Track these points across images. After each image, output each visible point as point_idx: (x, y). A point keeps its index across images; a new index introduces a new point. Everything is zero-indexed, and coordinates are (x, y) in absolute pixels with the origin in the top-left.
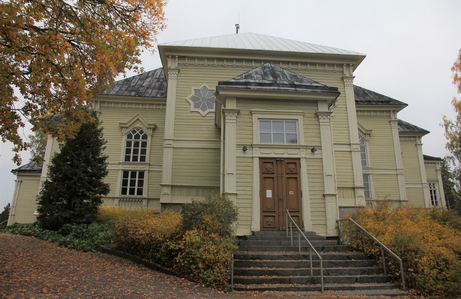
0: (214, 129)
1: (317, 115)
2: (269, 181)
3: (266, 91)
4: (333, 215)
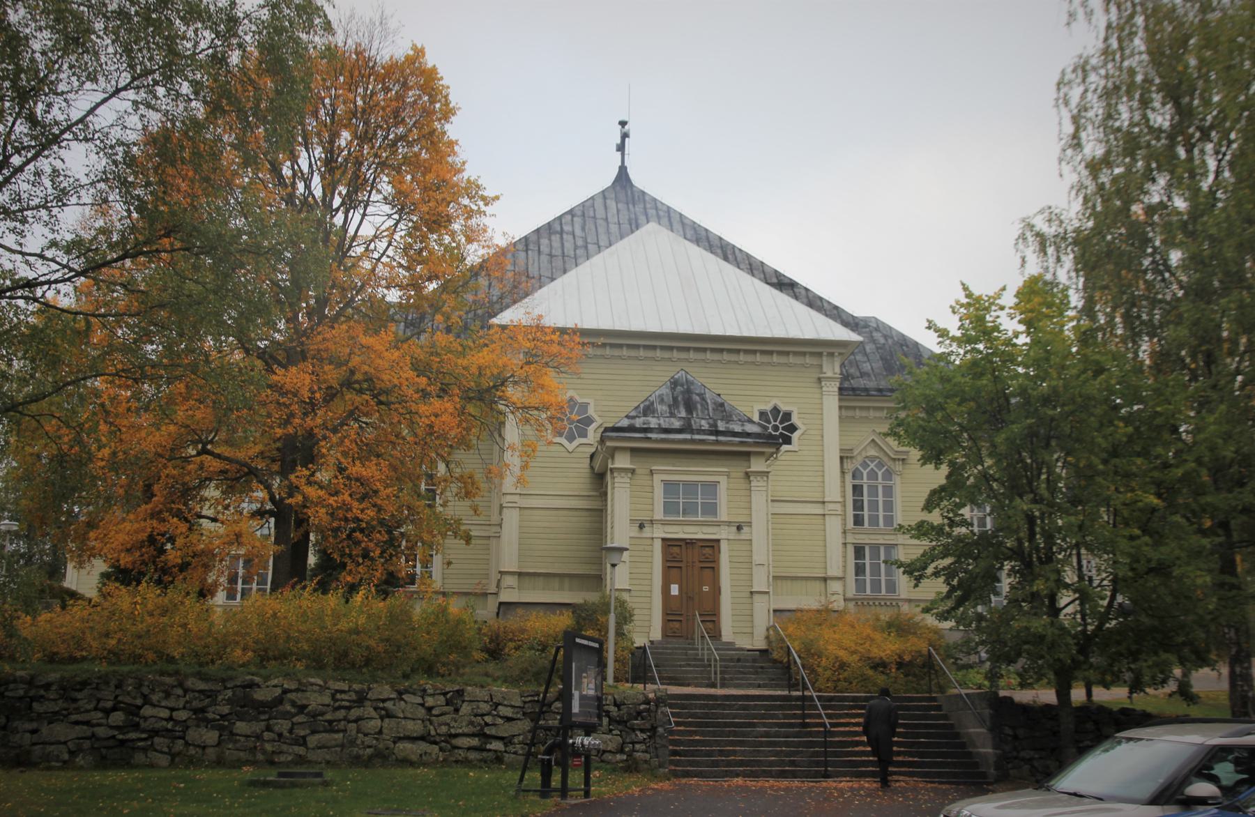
0: (588, 475)
1: (747, 475)
2: (675, 572)
3: (673, 441)
4: (762, 621)
